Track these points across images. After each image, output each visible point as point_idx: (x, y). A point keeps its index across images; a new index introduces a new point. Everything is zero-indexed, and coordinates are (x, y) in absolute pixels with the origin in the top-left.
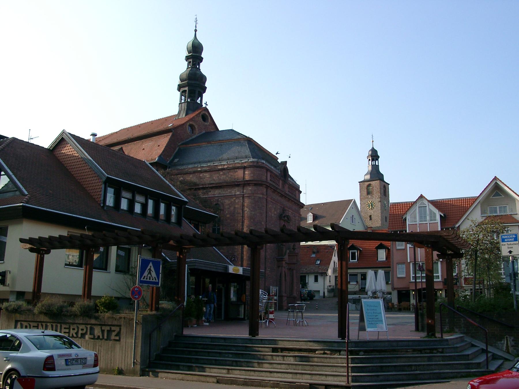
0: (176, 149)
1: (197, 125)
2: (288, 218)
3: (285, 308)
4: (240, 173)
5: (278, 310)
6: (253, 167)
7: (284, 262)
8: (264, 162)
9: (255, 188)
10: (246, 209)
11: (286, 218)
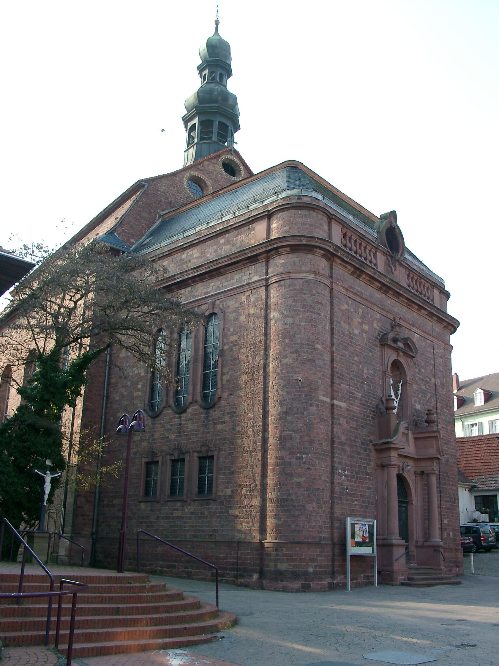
0: (154, 223)
1: (211, 179)
2: (406, 344)
3: (401, 578)
4: (260, 229)
5: (379, 583)
6: (288, 209)
7: (394, 454)
8: (320, 197)
9: (293, 258)
10: (273, 314)
11: (400, 345)
